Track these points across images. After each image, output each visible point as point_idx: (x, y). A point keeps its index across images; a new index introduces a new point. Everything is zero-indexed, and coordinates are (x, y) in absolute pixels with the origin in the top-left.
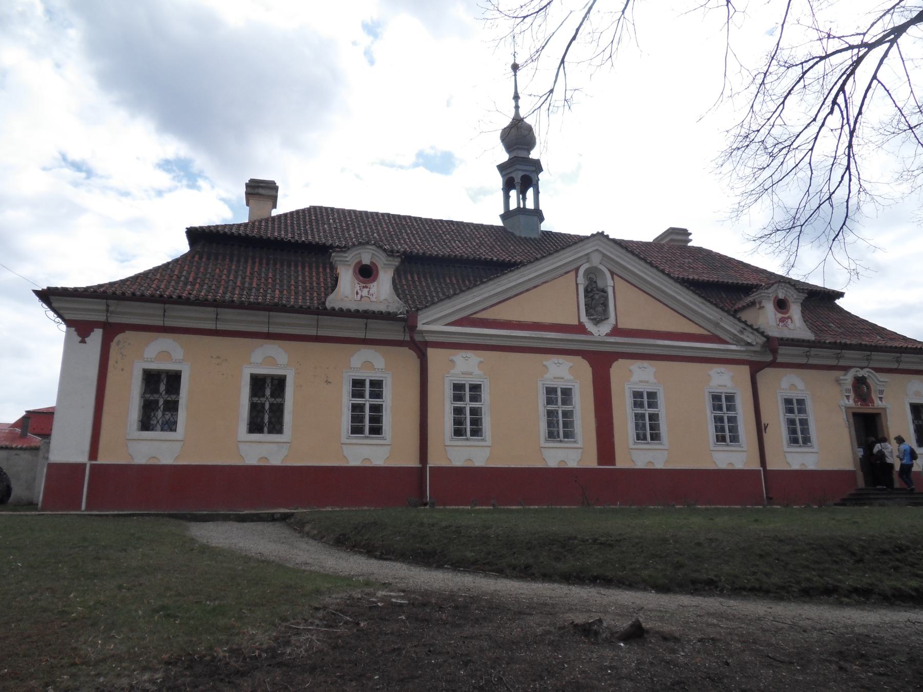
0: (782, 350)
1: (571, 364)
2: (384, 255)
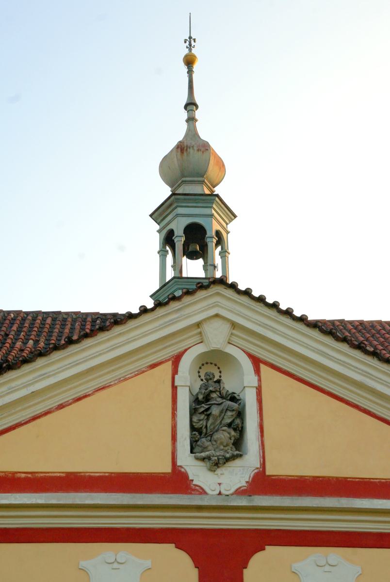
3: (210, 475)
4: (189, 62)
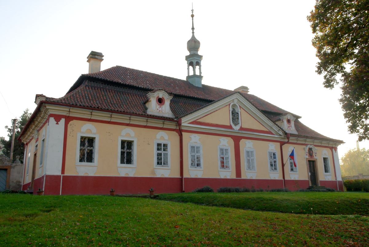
0: (291, 138)
2: (168, 94)
3: (235, 126)
4: (193, 16)
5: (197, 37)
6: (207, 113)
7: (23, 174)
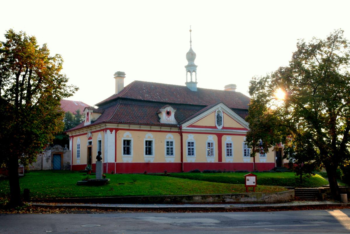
1: (213, 137)
5: (194, 50)
6: (199, 119)
7: (70, 157)
